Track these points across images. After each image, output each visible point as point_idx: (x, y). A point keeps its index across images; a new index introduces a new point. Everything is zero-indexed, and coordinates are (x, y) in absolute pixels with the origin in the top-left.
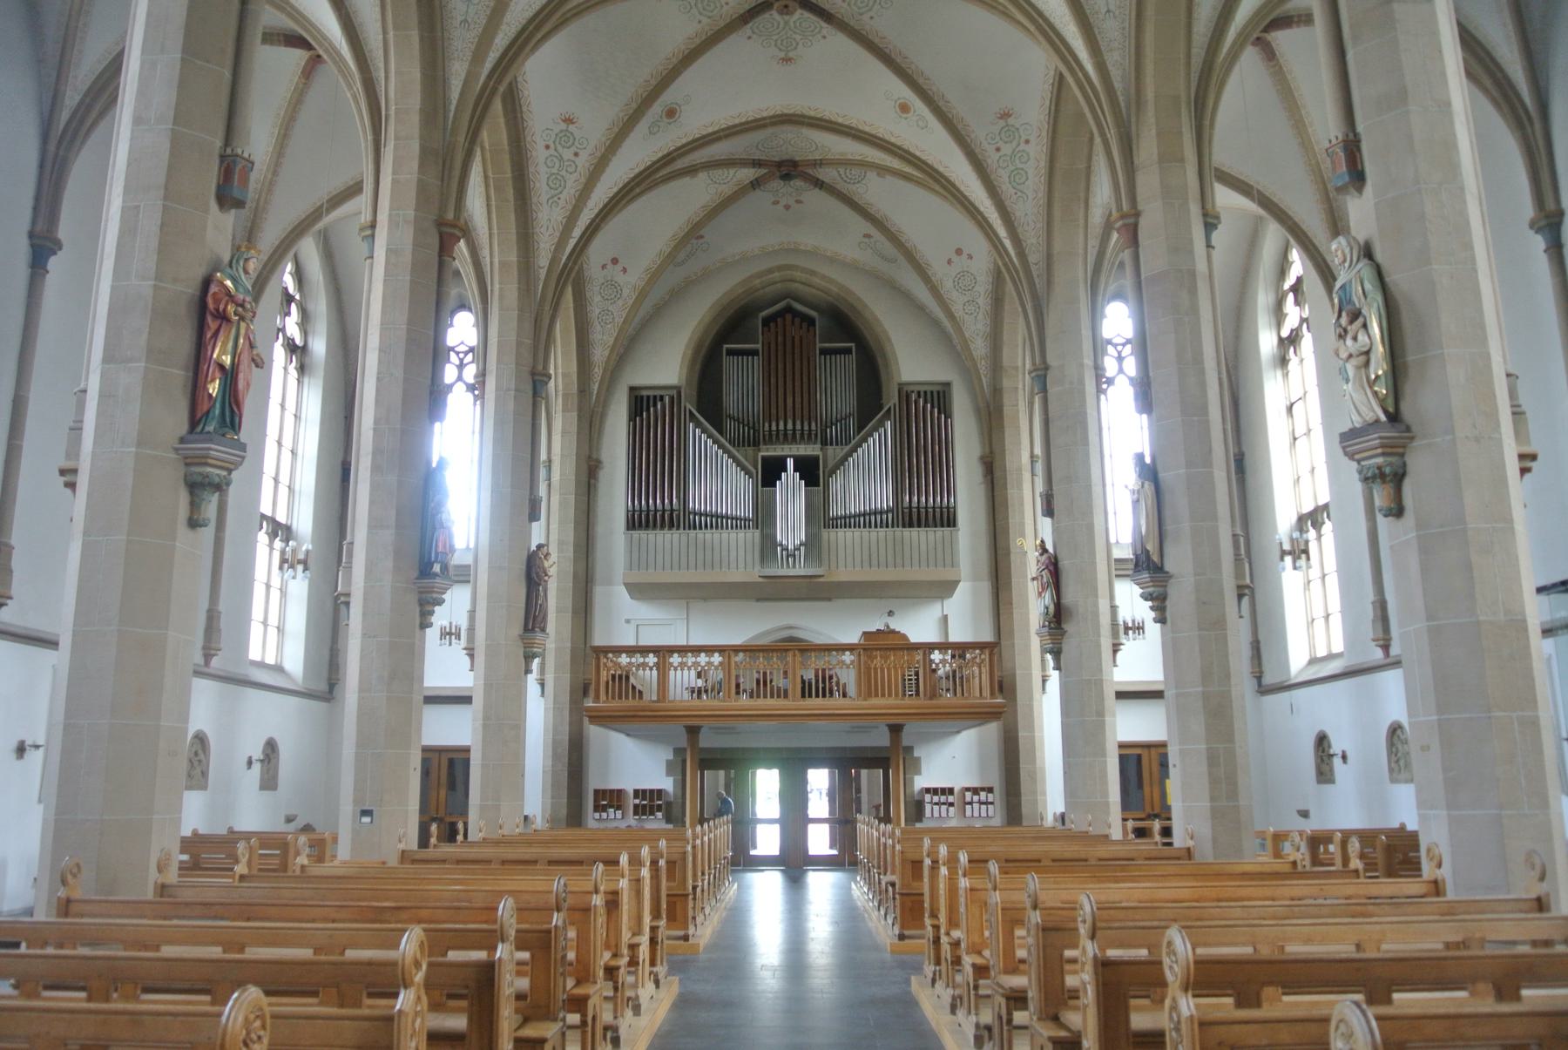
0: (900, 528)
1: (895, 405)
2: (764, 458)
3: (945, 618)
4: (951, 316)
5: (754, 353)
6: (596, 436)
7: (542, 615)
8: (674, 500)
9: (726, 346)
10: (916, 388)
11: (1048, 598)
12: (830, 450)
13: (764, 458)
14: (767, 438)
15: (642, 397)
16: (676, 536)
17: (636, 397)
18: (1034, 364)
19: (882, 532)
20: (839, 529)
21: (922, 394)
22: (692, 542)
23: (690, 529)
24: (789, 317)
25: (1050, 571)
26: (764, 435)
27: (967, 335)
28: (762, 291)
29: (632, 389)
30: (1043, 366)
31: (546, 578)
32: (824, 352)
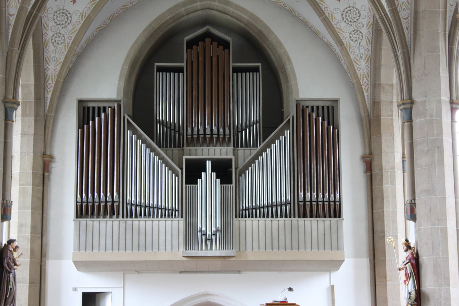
0: (297, 218)
1: (293, 117)
2: (187, 160)
3: (333, 287)
4: (340, 42)
5: (180, 70)
6: (49, 137)
7: (12, 297)
8: (115, 194)
9: (156, 64)
10: (310, 104)
11: (411, 286)
12: (241, 151)
13: (187, 160)
14: (190, 140)
15: (89, 108)
16: (116, 223)
17: (84, 108)
18: (402, 99)
19: (282, 221)
20: (247, 219)
21: (315, 109)
22: (129, 228)
23: (127, 217)
24: (208, 40)
25: (412, 265)
26: (187, 138)
27: (352, 57)
28: (186, 17)
29: (81, 102)
30: (409, 101)
31: (15, 267)
32: (236, 70)
